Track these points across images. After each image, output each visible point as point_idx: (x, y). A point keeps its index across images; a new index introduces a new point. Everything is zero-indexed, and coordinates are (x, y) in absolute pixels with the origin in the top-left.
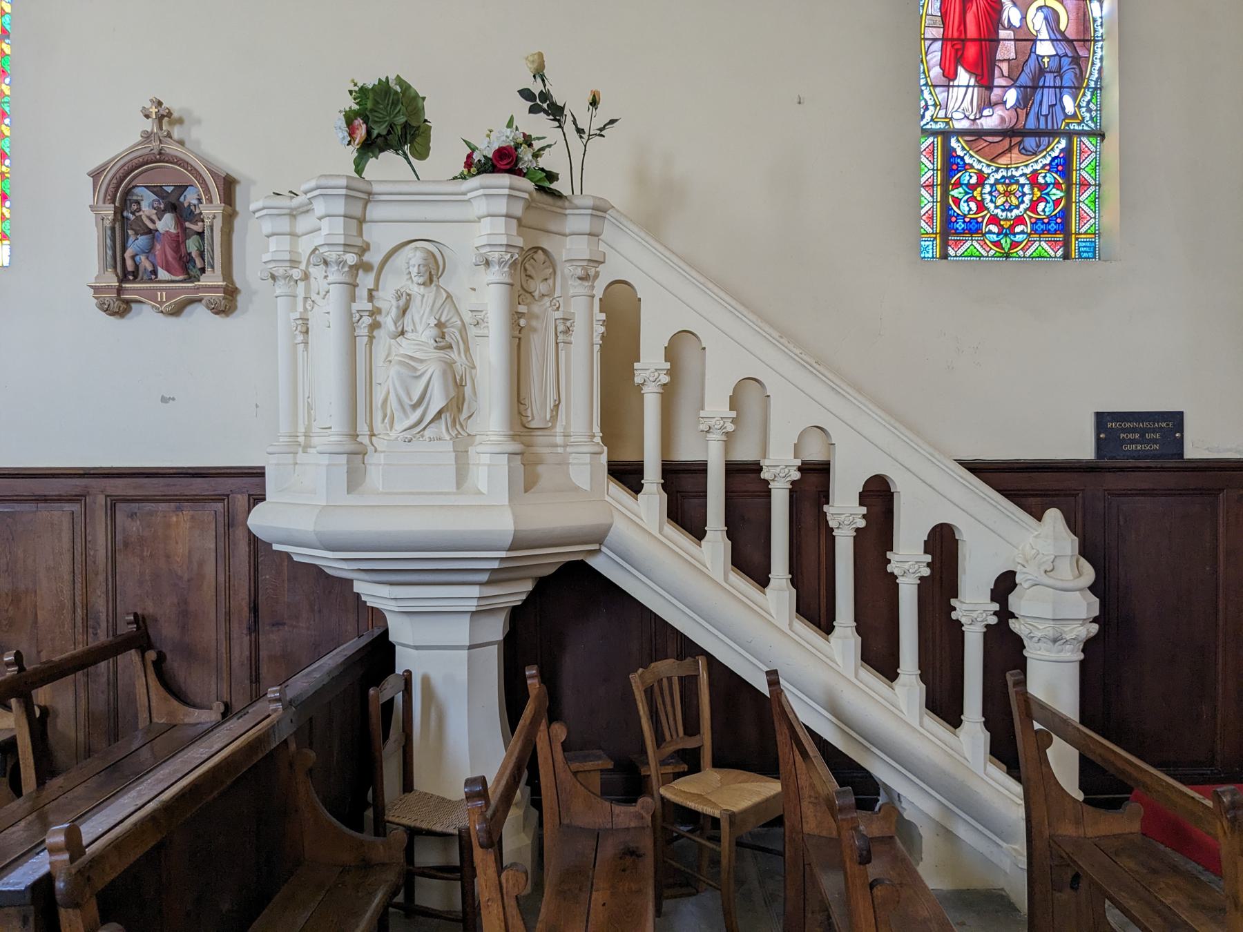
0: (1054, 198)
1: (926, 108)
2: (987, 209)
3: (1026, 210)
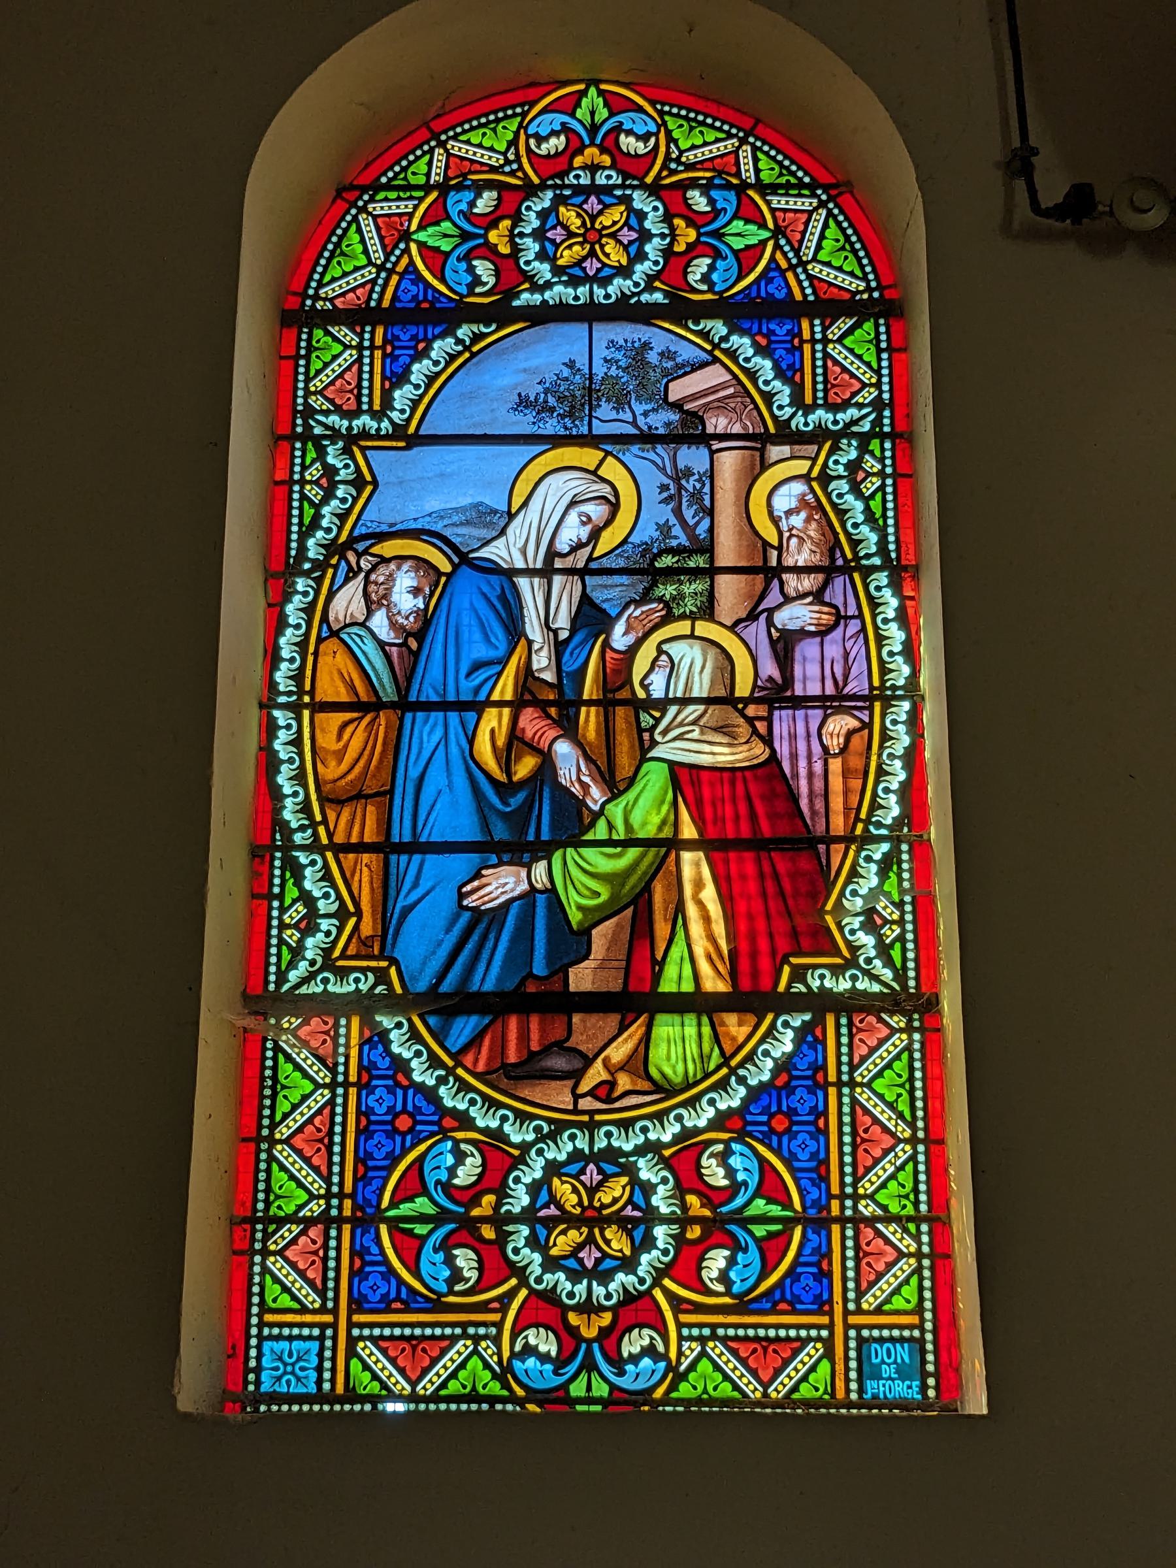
0: (738, 244)
1: (308, 926)
2: (521, 1272)
3: (659, 1274)
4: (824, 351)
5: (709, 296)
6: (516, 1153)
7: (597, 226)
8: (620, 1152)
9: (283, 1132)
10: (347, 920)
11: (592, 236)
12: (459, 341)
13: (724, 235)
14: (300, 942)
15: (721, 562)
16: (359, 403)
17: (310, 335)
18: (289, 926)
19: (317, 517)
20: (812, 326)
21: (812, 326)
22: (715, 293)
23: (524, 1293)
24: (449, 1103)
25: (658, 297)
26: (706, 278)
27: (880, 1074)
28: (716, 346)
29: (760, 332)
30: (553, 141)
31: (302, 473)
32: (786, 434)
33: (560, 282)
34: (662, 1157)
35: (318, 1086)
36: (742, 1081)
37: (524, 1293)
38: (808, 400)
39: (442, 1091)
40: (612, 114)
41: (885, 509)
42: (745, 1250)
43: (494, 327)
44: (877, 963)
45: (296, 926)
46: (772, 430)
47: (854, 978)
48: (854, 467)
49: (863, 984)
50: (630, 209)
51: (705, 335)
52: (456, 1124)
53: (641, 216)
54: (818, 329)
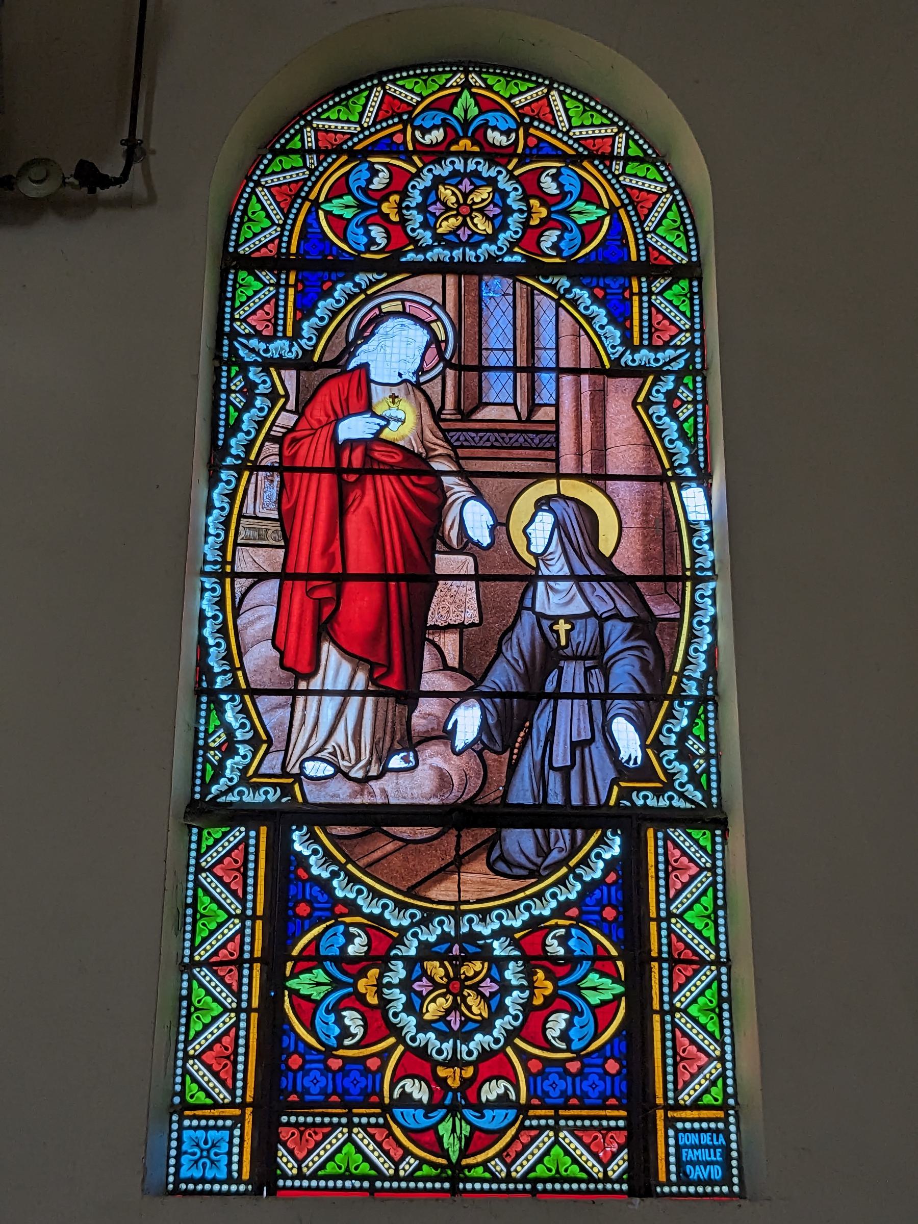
2: (397, 1031)
3: (510, 1035)
4: (649, 301)
5: (558, 260)
6: (395, 934)
7: (469, 202)
8: (480, 936)
9: (196, 1048)
10: (278, 400)
11: (465, 210)
12: (357, 285)
13: (570, 212)
14: (222, 762)
15: (563, 470)
16: (276, 331)
17: (236, 275)
18: (204, 870)
19: (239, 420)
20: (640, 283)
21: (640, 283)
22: (562, 258)
23: (401, 1048)
24: (339, 894)
25: (517, 258)
26: (555, 246)
27: (690, 908)
28: (562, 297)
29: (598, 286)
30: (435, 133)
31: (228, 384)
32: (618, 371)
33: (439, 245)
34: (513, 939)
35: (226, 1010)
36: (578, 878)
37: (401, 1048)
38: (636, 342)
39: (335, 883)
40: (481, 113)
41: (696, 429)
42: (581, 1014)
43: (384, 275)
44: (690, 787)
45: (219, 748)
46: (607, 365)
47: (671, 798)
48: (671, 396)
49: (678, 803)
50: (496, 190)
51: (552, 287)
52: (346, 911)
53: (504, 194)
54: (644, 285)
